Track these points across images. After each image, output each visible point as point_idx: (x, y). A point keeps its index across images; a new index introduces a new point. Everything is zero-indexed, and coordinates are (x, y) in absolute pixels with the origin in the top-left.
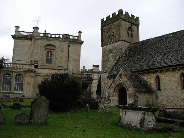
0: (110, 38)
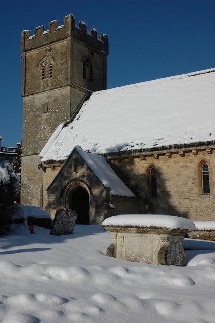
0: (43, 78)
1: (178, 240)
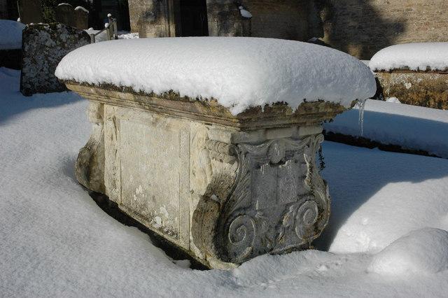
1: (293, 145)
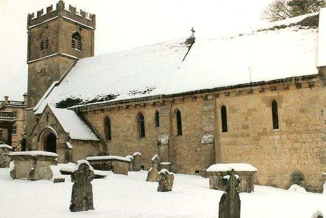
0: (42, 50)
